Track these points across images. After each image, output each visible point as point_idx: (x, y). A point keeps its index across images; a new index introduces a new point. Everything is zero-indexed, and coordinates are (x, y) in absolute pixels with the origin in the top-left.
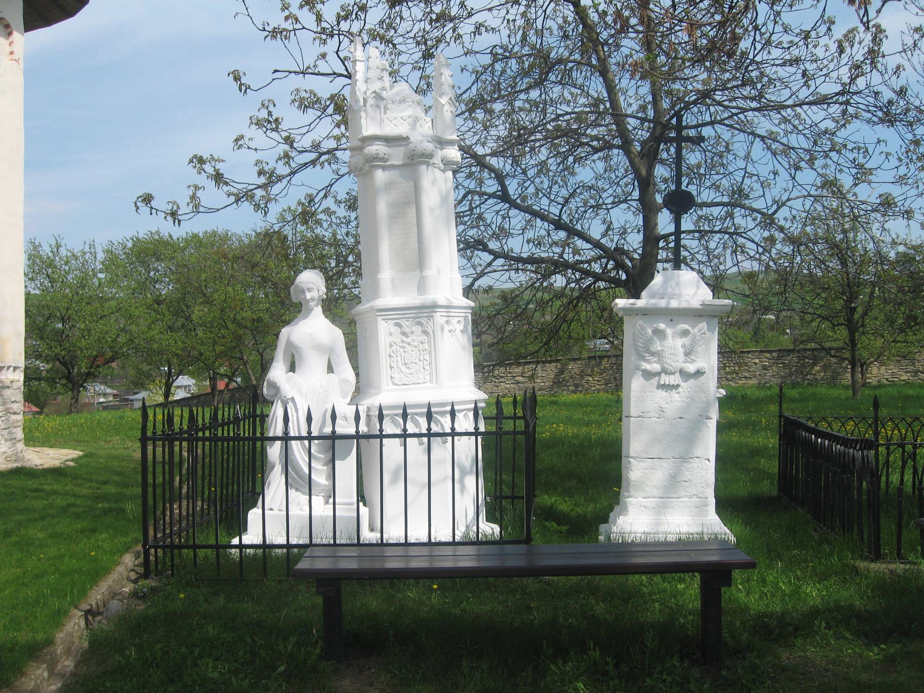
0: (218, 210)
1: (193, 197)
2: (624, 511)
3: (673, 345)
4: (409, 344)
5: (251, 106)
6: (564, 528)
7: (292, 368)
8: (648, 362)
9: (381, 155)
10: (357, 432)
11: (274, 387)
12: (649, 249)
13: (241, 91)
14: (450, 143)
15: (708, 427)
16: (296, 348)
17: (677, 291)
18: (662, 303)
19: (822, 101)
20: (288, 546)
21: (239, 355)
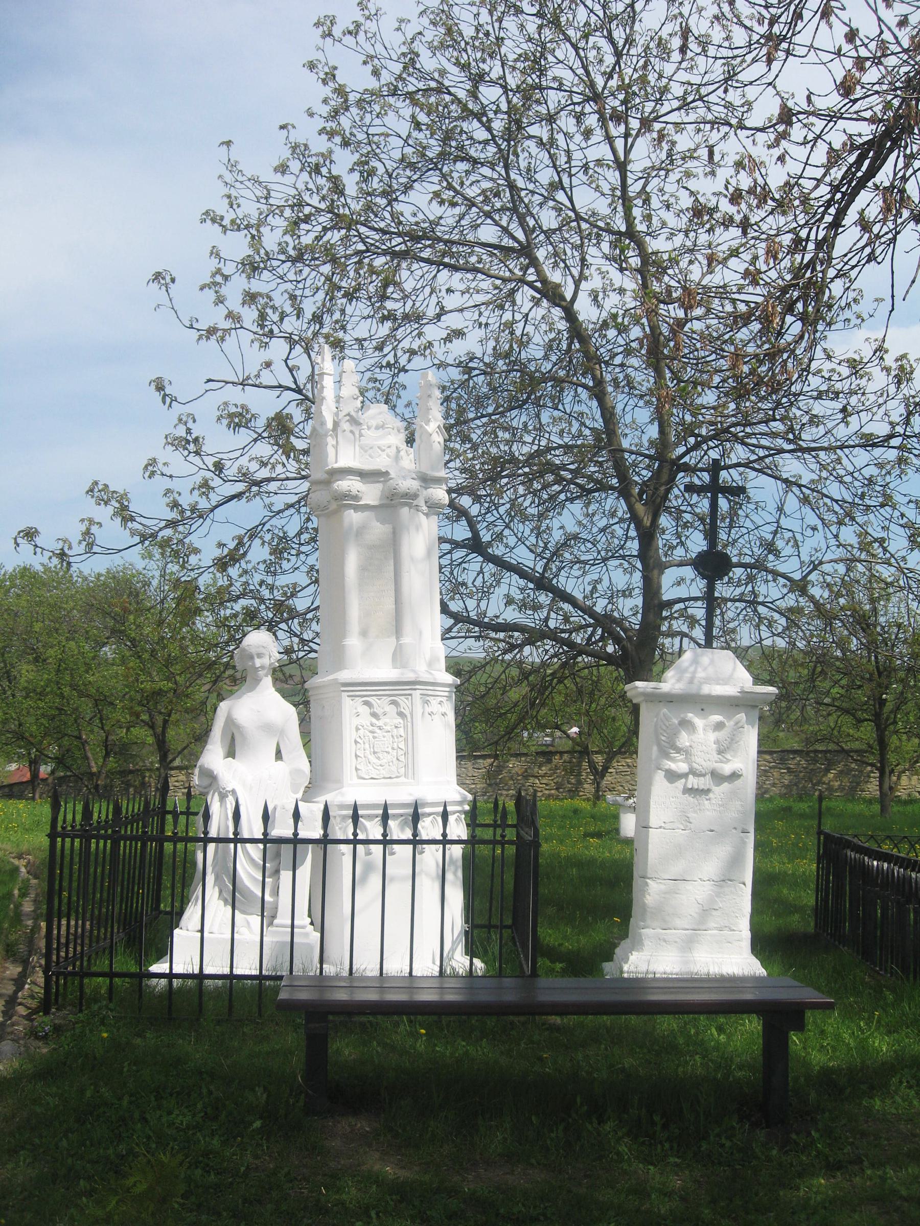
0: (120, 551)
1: (87, 533)
2: (638, 944)
4: (380, 728)
5: (166, 422)
6: (559, 966)
7: (231, 753)
8: (673, 760)
9: (354, 492)
10: (296, 834)
11: (211, 777)
12: (651, 617)
13: (164, 403)
14: (438, 481)
16: (238, 727)
19: (869, 442)
20: (231, 977)
21: (76, 733)
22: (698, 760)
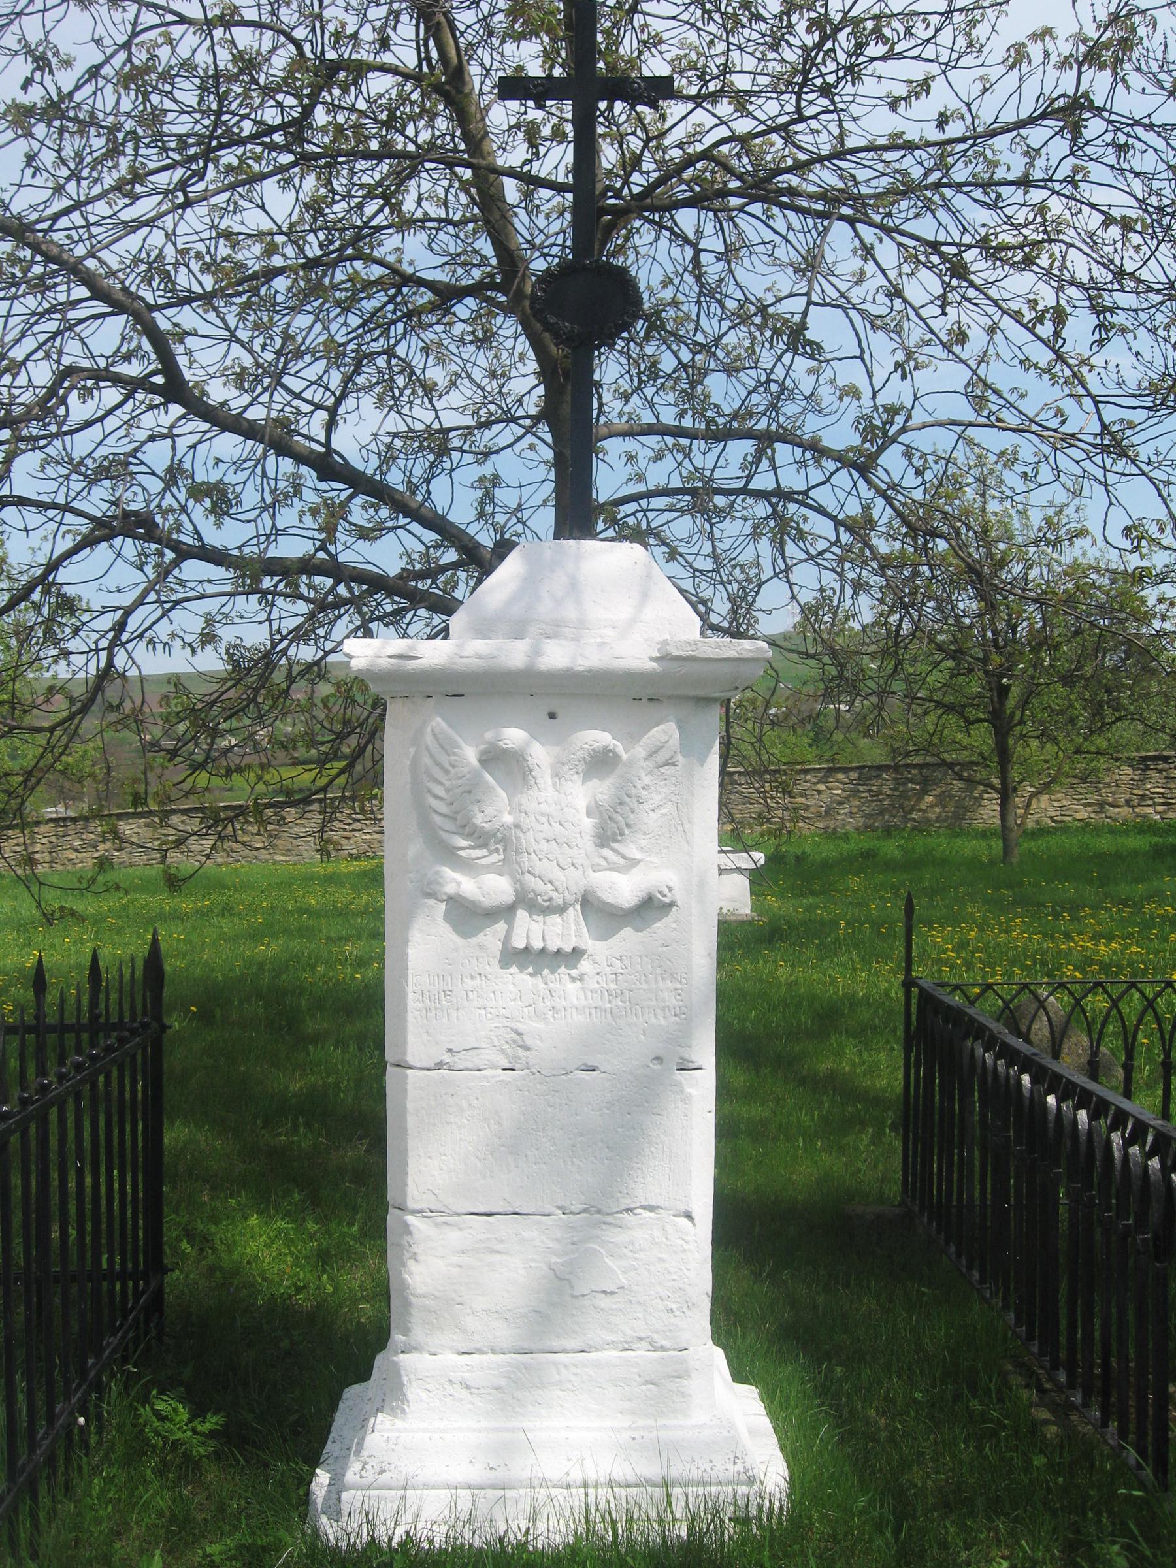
2: (393, 1397)
3: (553, 802)
15: (687, 1099)
17: (570, 612)
18: (514, 654)
22: (541, 867)
